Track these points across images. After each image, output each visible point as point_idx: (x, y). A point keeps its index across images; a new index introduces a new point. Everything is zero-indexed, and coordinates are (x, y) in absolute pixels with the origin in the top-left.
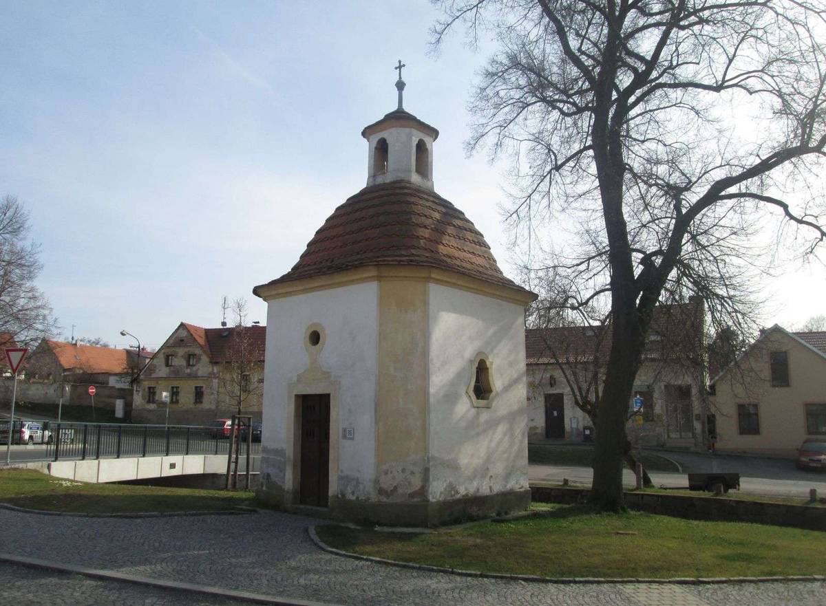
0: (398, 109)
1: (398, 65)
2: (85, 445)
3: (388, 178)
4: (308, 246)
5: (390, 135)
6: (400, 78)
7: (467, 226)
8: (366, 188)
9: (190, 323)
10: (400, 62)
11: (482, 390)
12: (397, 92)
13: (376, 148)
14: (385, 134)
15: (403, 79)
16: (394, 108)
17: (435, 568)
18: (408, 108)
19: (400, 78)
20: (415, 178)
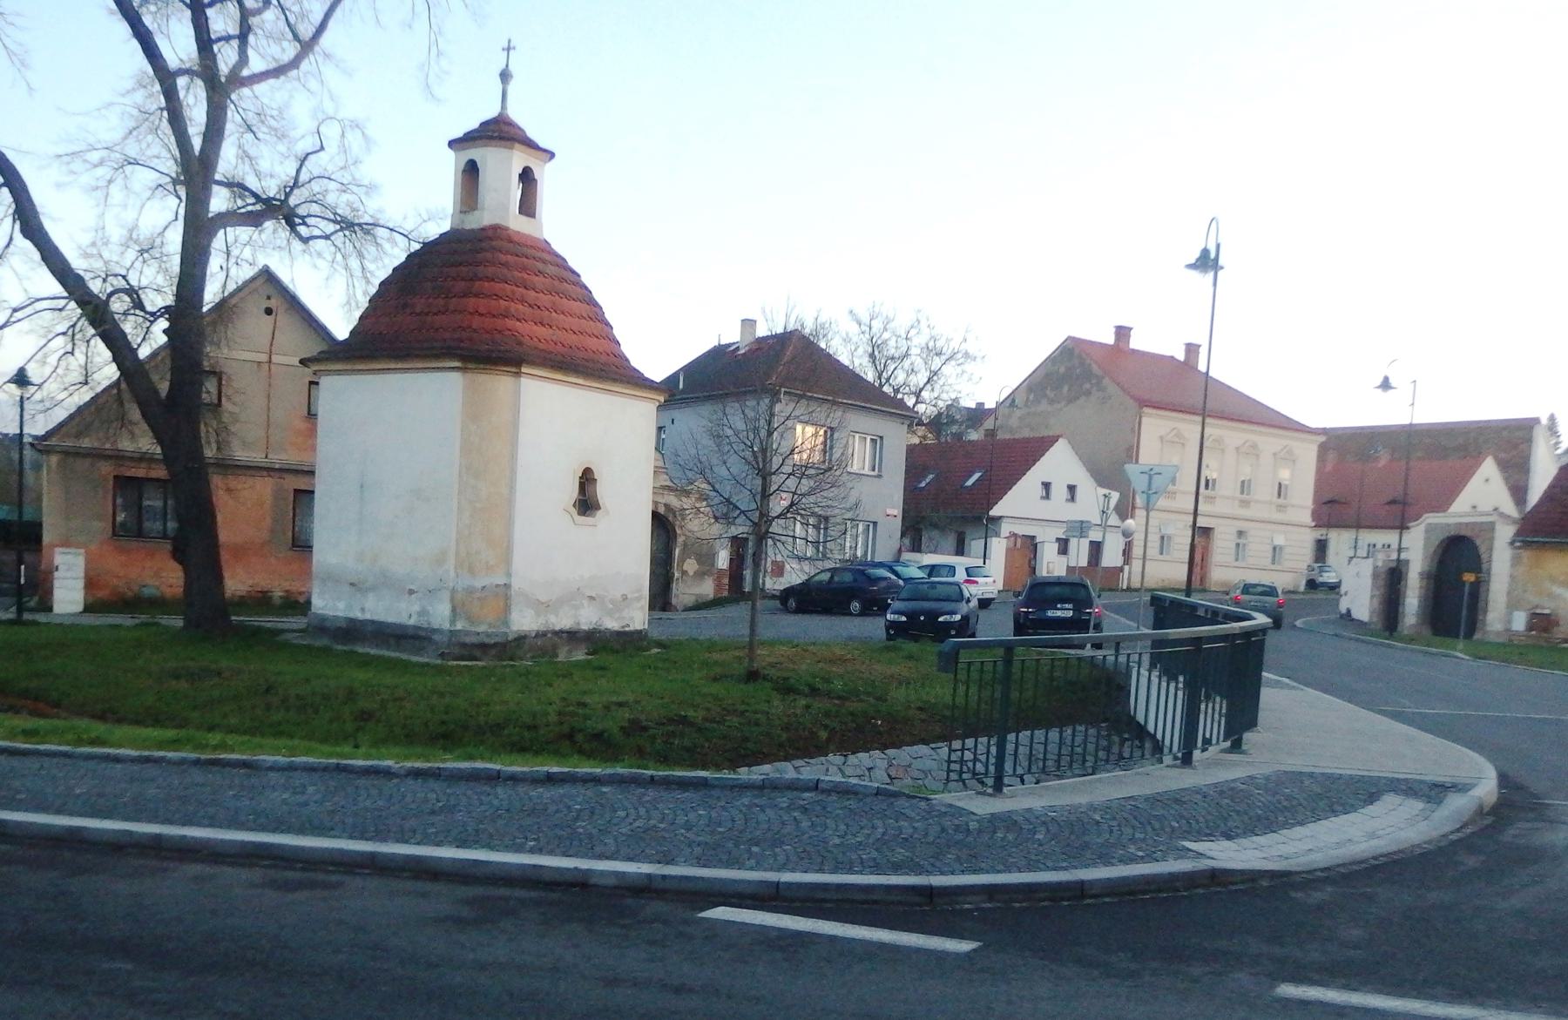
0: (500, 115)
1: (506, 46)
2: (165, 524)
3: (475, 221)
4: (393, 270)
5: (481, 154)
6: (507, 66)
7: (572, 277)
8: (448, 232)
9: (316, 505)
10: (509, 41)
11: (586, 503)
12: (500, 86)
13: (464, 171)
14: (475, 153)
15: (511, 67)
16: (491, 112)
17: (1107, 900)
18: (516, 114)
19: (507, 66)
20: (517, 223)
